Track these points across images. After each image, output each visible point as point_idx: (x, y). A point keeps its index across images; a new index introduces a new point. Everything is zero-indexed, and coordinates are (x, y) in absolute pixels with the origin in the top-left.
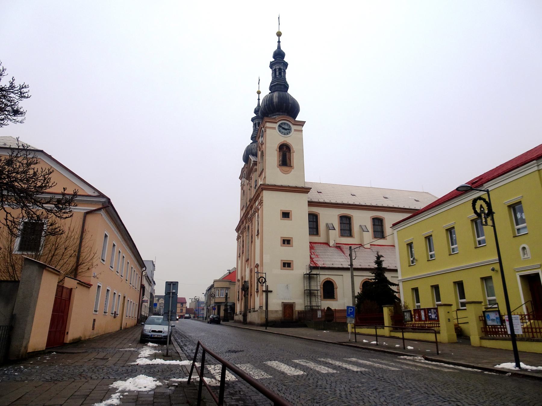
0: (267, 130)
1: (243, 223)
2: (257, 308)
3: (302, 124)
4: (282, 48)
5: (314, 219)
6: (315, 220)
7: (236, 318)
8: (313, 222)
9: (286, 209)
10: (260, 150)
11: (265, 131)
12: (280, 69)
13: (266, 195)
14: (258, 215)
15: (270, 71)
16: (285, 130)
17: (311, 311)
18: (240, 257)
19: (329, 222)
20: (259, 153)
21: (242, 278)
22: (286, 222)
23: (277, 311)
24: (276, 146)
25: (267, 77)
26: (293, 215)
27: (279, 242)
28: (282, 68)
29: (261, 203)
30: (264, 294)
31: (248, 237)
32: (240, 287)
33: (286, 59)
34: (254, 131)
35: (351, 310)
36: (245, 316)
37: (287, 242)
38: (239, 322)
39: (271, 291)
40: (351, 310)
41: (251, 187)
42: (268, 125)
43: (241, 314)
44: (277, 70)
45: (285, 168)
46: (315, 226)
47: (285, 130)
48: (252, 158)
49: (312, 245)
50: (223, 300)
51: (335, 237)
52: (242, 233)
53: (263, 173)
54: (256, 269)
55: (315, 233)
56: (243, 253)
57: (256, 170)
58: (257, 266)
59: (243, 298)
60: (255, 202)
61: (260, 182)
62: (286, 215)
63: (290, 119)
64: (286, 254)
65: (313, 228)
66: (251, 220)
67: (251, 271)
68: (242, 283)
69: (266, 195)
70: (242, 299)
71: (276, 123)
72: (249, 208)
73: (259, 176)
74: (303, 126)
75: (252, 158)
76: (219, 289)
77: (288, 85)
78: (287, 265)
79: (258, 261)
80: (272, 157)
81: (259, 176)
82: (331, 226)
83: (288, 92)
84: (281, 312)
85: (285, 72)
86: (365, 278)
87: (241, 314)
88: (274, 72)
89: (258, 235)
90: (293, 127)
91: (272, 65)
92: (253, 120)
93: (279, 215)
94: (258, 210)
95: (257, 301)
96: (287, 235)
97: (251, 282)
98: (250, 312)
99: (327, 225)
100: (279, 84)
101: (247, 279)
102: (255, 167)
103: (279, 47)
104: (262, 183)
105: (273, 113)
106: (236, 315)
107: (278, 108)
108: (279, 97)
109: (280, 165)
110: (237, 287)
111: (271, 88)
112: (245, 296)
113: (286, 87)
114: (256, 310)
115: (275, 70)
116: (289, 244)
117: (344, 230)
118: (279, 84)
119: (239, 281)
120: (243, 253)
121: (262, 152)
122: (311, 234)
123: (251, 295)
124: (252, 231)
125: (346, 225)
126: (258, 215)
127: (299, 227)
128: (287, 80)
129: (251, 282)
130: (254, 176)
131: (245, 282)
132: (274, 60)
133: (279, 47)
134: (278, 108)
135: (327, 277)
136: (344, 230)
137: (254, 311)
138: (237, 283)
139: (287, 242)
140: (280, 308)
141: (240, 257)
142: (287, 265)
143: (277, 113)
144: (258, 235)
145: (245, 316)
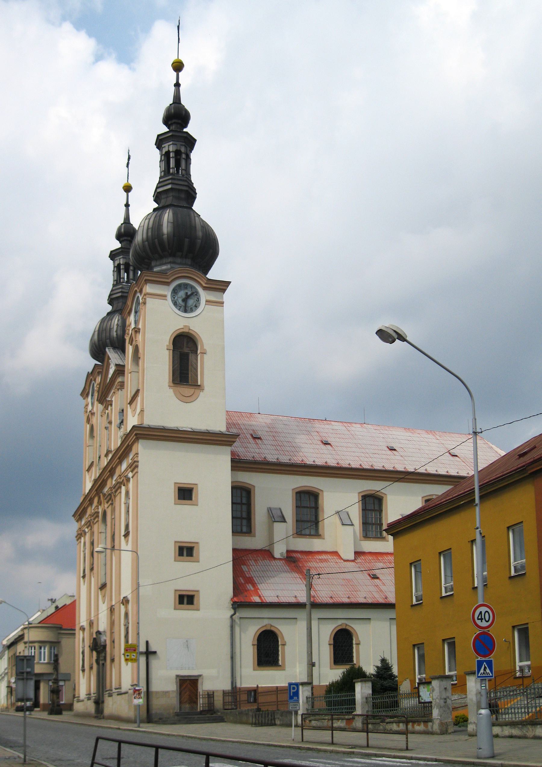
0: (149, 300)
1: (91, 503)
2: (126, 685)
3: (221, 286)
4: (183, 102)
5: (242, 498)
6: (244, 501)
7: (78, 707)
8: (242, 504)
9: (186, 480)
10: (131, 343)
11: (145, 303)
12: (178, 153)
13: (144, 451)
14: (127, 493)
15: (156, 154)
16: (186, 303)
17: (235, 694)
18: (84, 577)
19: (274, 505)
20: (130, 349)
21: (91, 624)
22: (185, 508)
23: (166, 693)
24: (166, 340)
25: (149, 173)
26: (201, 494)
27: (171, 551)
28: (183, 150)
29: (134, 466)
30: (143, 660)
31: (103, 535)
32: (87, 643)
33: (190, 129)
34: (117, 282)
35: (294, 688)
36: (99, 703)
37: (186, 551)
38: (84, 715)
39: (155, 653)
40: (294, 688)
41: (110, 423)
42: (149, 288)
43: (89, 699)
44: (172, 155)
45: (186, 390)
46: (244, 515)
47: (186, 303)
48: (113, 357)
49: (240, 557)
50: (47, 669)
51: (283, 537)
52: (89, 524)
53: (139, 399)
54: (123, 607)
55: (244, 529)
56: (92, 569)
57: (122, 386)
58: (125, 601)
59: (95, 666)
60: (120, 463)
61: (132, 421)
62: (185, 494)
63: (196, 274)
64: (186, 576)
65: (242, 518)
66: (111, 498)
67: (112, 610)
68: (91, 634)
69: (144, 451)
70: (91, 668)
71: (168, 284)
72: (107, 473)
73: (131, 403)
74: (224, 291)
75: (113, 357)
76: (37, 645)
77: (194, 190)
78: (186, 599)
79: (126, 591)
80: (157, 361)
81: (131, 403)
82: (277, 513)
83: (197, 207)
84: (174, 695)
85: (188, 159)
86: (340, 622)
87: (89, 699)
88: (166, 157)
89: (126, 535)
90: (204, 295)
91: (160, 142)
92: (113, 255)
93: (171, 493)
94: (128, 480)
95: (125, 674)
96: (186, 538)
97: (112, 633)
98: (110, 695)
99: (270, 510)
100: (176, 190)
101: (103, 625)
102: (120, 379)
103: (177, 98)
104: (136, 423)
105: (161, 257)
106: (79, 701)
107: (170, 248)
108: (176, 224)
109: (179, 499)
110: (81, 642)
111: (157, 197)
112: (97, 661)
113: (190, 195)
114: (123, 690)
115: (167, 154)
116: (190, 498)
117: (302, 521)
118: (176, 190)
119: (83, 629)
120: (92, 569)
121: (136, 350)
122: (235, 532)
123: (113, 660)
124: (113, 526)
125: (308, 508)
126: (127, 493)
127: (211, 523)
128: (193, 179)
129: (112, 633)
130: (118, 399)
131: (98, 633)
132: (165, 129)
133: (177, 98)
134: (170, 248)
135: (266, 622)
136: (302, 521)
137: (120, 694)
138: (80, 635)
139: (186, 551)
140: (172, 687)
141: (84, 577)
142: (186, 599)
143: (170, 259)
144: (126, 535)
145: (99, 703)
